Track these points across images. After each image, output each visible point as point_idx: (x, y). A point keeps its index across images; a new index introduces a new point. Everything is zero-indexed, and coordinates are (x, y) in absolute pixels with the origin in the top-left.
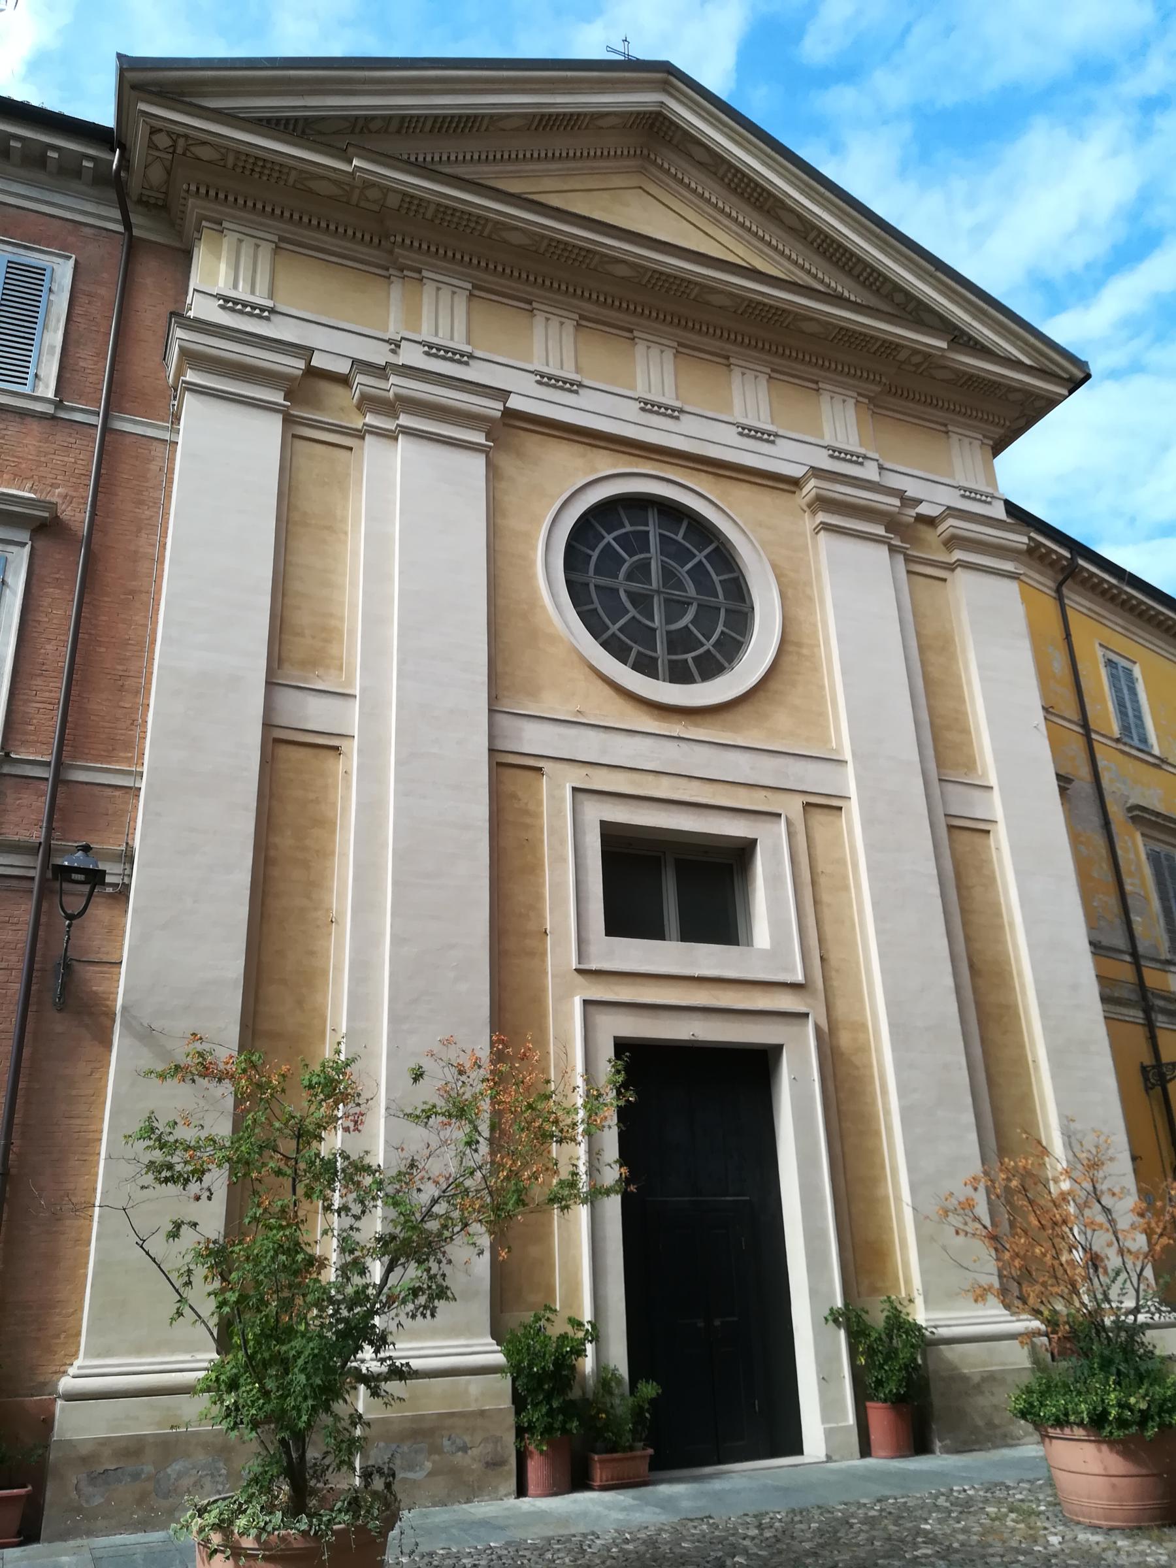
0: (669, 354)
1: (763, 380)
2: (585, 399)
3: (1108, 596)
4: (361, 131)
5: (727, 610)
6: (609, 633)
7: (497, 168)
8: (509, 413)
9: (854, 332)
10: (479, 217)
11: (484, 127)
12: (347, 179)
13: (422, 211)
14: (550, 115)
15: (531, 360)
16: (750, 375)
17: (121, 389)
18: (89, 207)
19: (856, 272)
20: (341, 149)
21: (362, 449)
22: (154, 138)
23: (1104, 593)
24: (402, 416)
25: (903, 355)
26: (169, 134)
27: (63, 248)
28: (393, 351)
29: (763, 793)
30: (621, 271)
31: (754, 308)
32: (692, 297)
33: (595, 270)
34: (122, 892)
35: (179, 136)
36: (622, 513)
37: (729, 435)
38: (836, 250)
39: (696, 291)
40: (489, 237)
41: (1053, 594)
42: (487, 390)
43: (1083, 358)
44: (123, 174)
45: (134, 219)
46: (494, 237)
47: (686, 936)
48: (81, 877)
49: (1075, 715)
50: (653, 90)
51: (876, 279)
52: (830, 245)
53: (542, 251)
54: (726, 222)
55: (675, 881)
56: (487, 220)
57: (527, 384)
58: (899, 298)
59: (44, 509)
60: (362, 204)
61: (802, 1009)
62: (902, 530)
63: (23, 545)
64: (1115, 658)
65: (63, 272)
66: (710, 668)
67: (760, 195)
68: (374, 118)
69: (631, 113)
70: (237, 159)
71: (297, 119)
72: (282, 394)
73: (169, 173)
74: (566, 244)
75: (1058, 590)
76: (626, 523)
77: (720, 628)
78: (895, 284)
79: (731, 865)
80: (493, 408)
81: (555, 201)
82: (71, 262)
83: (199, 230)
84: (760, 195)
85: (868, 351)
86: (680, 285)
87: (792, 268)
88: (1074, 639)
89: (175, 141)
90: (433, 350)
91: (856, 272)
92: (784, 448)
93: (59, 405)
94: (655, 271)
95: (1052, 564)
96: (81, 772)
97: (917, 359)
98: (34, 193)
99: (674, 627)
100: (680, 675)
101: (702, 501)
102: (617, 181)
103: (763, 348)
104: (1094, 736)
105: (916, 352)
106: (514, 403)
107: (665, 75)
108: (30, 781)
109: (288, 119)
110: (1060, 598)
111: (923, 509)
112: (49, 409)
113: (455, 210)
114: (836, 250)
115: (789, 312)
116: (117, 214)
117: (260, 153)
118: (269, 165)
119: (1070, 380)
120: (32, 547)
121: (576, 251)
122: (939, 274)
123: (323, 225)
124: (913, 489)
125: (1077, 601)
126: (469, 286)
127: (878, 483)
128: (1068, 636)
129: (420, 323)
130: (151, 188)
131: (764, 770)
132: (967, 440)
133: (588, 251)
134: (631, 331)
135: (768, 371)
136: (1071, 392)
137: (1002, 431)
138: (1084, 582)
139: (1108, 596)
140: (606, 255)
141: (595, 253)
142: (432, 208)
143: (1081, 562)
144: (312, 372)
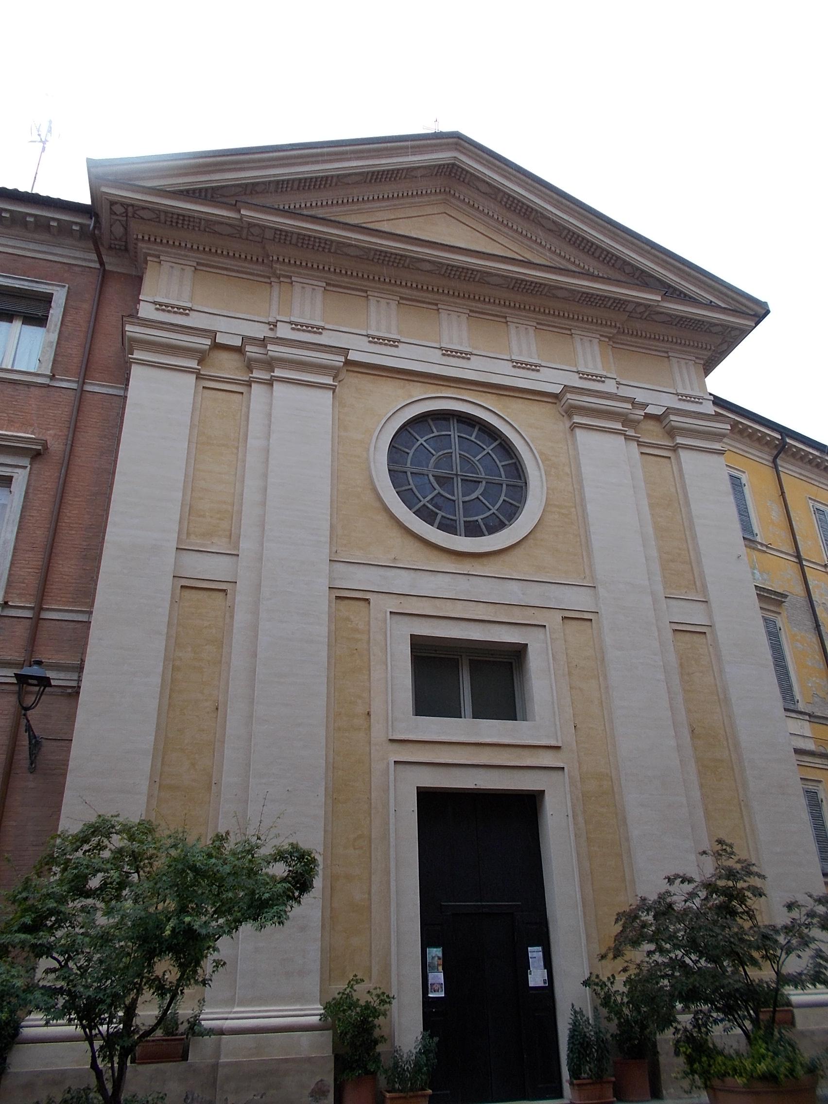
0: (464, 317)
1: (531, 330)
2: (402, 350)
3: (814, 463)
4: (251, 193)
5: (507, 485)
6: (421, 504)
7: (345, 209)
8: (348, 363)
9: (593, 294)
10: (326, 240)
11: (334, 184)
12: (237, 223)
13: (402, 262)
14: (378, 172)
15: (366, 328)
16: (522, 328)
17: (98, 365)
18: (78, 254)
19: (597, 255)
20: (231, 205)
21: (250, 393)
22: (113, 208)
23: (810, 462)
24: (276, 370)
25: (630, 308)
26: (122, 204)
27: (61, 280)
28: (271, 329)
29: (533, 610)
30: (427, 267)
31: (520, 284)
32: (477, 279)
33: (408, 267)
34: (74, 693)
35: (128, 205)
36: (431, 423)
37: (507, 368)
38: (582, 242)
39: (546, 290)
40: (335, 253)
41: (771, 465)
42: (333, 349)
43: (763, 300)
44: (96, 232)
45: (105, 259)
46: (339, 252)
47: (479, 713)
48: (35, 682)
49: (789, 548)
50: (450, 150)
51: (611, 258)
52: (577, 239)
53: (371, 258)
54: (506, 230)
55: (469, 674)
56: (332, 241)
57: (363, 343)
58: (628, 269)
59: (37, 444)
60: (250, 238)
61: (561, 765)
62: (628, 422)
63: (25, 467)
64: (822, 507)
65: (59, 296)
66: (496, 526)
67: (526, 210)
68: (258, 184)
69: (435, 166)
70: (166, 216)
71: (206, 189)
72: (196, 362)
73: (126, 229)
74: (386, 252)
75: (774, 462)
76: (435, 430)
77: (503, 498)
78: (625, 261)
79: (511, 663)
80: (338, 360)
81: (385, 227)
82: (66, 288)
83: (146, 262)
84: (526, 210)
85: (605, 307)
86: (467, 273)
87: (558, 259)
88: (787, 495)
89: (126, 209)
90: (296, 326)
91: (597, 255)
92: (545, 374)
93: (53, 377)
94: (448, 265)
95: (767, 443)
96: (47, 612)
97: (641, 309)
98: (44, 248)
99: (467, 499)
100: (473, 530)
101: (488, 413)
102: (429, 210)
103: (578, 319)
104: (804, 563)
105: (639, 304)
106: (353, 356)
107: (457, 141)
108: (20, 620)
109: (200, 190)
110: (776, 467)
111: (649, 410)
112: (46, 381)
113: (310, 236)
114: (582, 242)
115: (545, 285)
116: (94, 257)
117: (180, 212)
118: (186, 218)
119: (755, 315)
120: (31, 468)
121: (393, 256)
122: (653, 251)
123: (377, 278)
124: (640, 396)
125: (789, 470)
126: (324, 285)
127: (616, 395)
128: (783, 493)
129: (302, 311)
130: (116, 239)
131: (534, 595)
132: (683, 362)
133: (401, 256)
134: (437, 305)
135: (535, 324)
136: (757, 324)
137: (709, 354)
138: (794, 455)
139: (814, 463)
140: (414, 258)
141: (406, 256)
142: (295, 237)
143: (788, 441)
144: (217, 346)
